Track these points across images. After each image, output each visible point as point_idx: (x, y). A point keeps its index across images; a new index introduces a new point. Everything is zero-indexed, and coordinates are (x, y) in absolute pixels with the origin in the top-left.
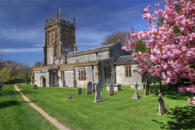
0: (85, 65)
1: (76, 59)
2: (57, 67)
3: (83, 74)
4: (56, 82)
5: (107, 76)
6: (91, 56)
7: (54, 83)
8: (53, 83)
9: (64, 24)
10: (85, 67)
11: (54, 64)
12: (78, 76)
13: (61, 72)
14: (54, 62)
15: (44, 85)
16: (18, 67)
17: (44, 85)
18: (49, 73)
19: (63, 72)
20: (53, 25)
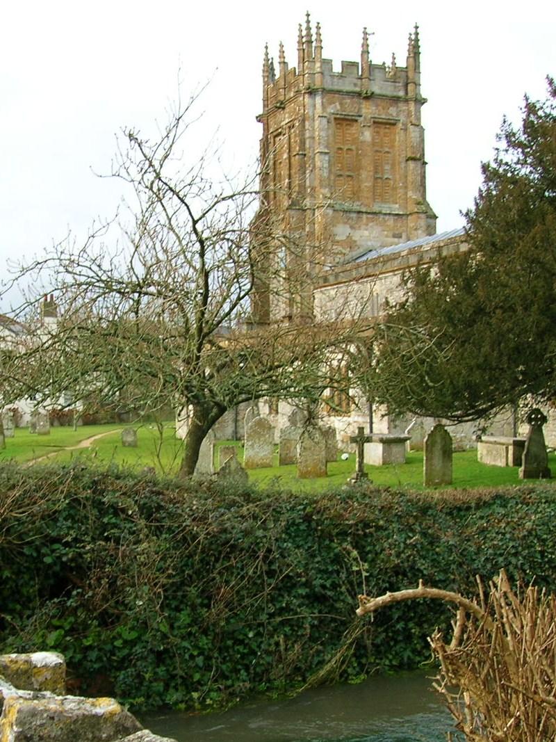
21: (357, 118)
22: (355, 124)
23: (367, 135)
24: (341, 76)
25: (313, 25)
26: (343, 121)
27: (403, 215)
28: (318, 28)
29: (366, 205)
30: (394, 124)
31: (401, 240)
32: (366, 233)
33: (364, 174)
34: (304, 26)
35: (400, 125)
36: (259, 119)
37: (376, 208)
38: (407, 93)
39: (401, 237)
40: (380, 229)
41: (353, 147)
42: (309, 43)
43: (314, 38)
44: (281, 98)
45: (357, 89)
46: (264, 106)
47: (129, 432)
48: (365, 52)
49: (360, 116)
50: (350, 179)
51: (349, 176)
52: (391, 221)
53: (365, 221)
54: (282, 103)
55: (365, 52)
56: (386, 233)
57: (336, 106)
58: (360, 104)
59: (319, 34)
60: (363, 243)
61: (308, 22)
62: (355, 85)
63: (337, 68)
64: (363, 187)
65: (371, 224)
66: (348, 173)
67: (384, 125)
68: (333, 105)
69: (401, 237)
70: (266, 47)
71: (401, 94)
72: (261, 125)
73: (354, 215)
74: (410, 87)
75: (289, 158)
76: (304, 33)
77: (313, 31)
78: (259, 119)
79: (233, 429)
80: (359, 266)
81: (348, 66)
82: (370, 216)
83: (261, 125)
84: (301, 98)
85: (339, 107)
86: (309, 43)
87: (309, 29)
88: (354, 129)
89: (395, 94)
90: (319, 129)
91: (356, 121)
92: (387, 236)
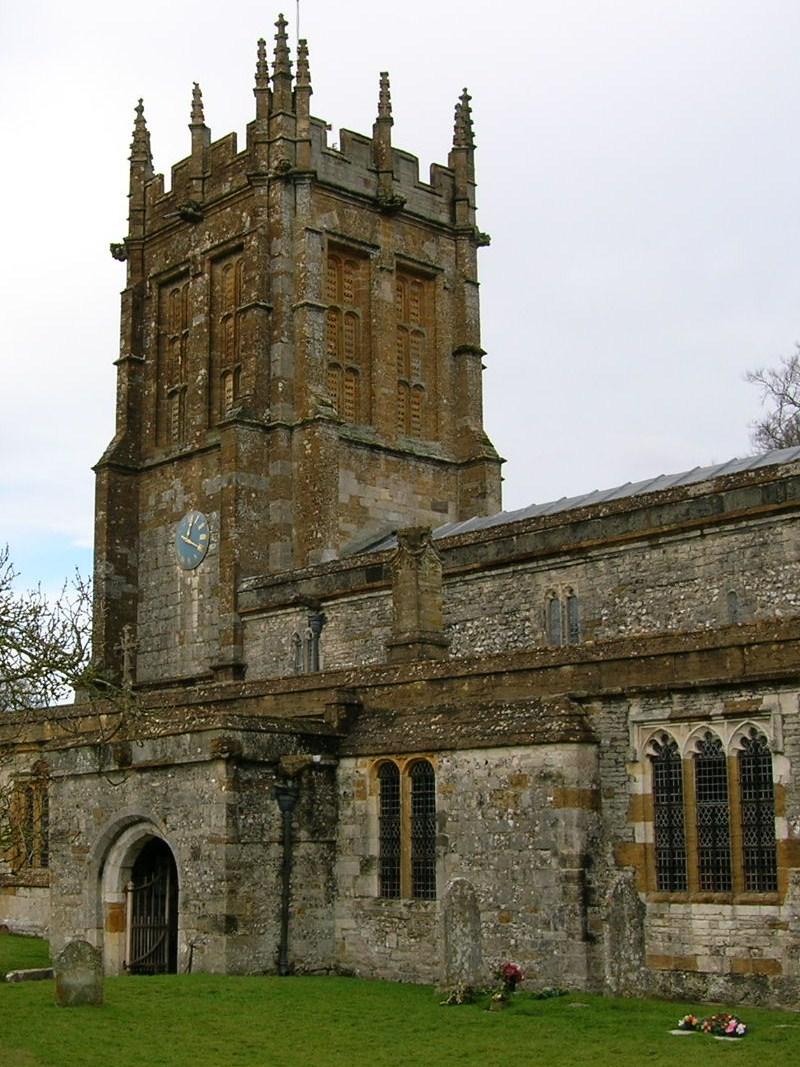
0: (766, 665)
1: (540, 599)
2: (332, 696)
3: (735, 792)
4: (310, 903)
5: (406, 882)
6: (768, 555)
7: (285, 917)
8: (274, 928)
9: (360, 188)
10: (768, 699)
11: (239, 669)
12: (644, 832)
13: (388, 776)
14: (238, 637)
15: (155, 955)
16: (397, 198)
17: (155, 955)
18: (235, 784)
19: (424, 777)
20: (220, 202)
21: (369, 250)
22: (362, 264)
23: (386, 290)
24: (341, 158)
25: (292, 44)
26: (345, 252)
27: (451, 463)
28: (303, 50)
29: (384, 436)
30: (431, 277)
31: (447, 517)
32: (385, 494)
33: (381, 370)
34: (271, 46)
35: (441, 280)
36: (118, 252)
37: (402, 444)
38: (453, 218)
39: (445, 511)
40: (409, 488)
41: (358, 311)
42: (283, 85)
43: (294, 70)
44: (196, 197)
45: (371, 192)
46: (133, 220)
47: (81, 957)
48: (384, 122)
49: (376, 247)
50: (350, 376)
51: (351, 370)
52: (428, 474)
53: (383, 467)
54: (198, 208)
55: (384, 122)
56: (420, 498)
57: (332, 217)
58: (374, 223)
59: (303, 64)
60: (380, 515)
61: (282, 37)
62: (366, 182)
63: (333, 140)
64: (378, 395)
65: (394, 476)
66: (350, 363)
67: (414, 274)
68: (326, 215)
69: (445, 511)
70: (140, 109)
71: (444, 218)
72: (122, 267)
73: (364, 453)
74: (460, 209)
75: (211, 324)
76: (271, 58)
77: (293, 56)
78: (118, 252)
79: (278, 940)
80: (368, 555)
81: (349, 138)
82: (391, 458)
83: (122, 267)
84: (262, 191)
85: (337, 221)
86: (283, 85)
87: (282, 50)
88: (359, 274)
89: (434, 217)
90: (303, 257)
91: (366, 257)
92: (422, 506)
